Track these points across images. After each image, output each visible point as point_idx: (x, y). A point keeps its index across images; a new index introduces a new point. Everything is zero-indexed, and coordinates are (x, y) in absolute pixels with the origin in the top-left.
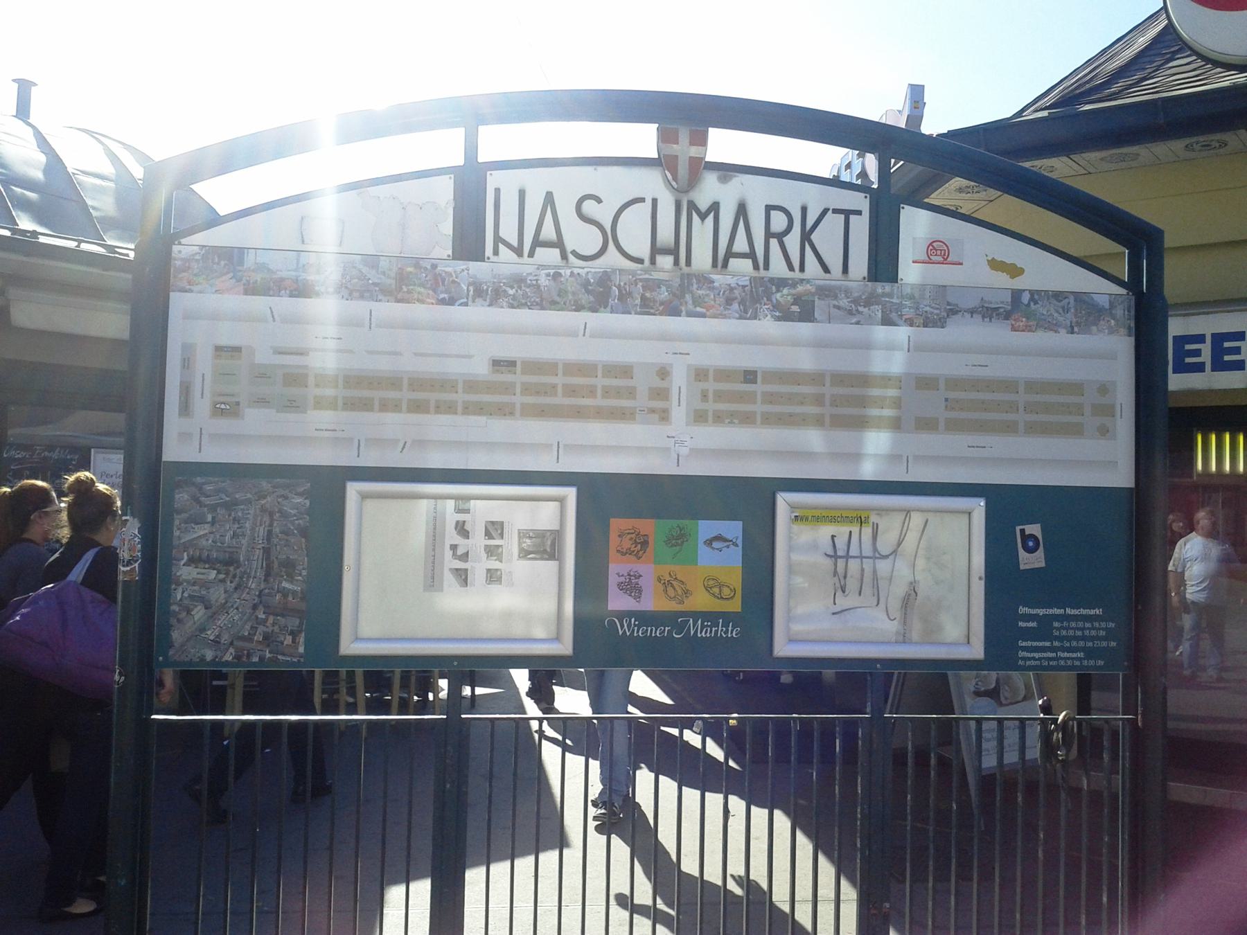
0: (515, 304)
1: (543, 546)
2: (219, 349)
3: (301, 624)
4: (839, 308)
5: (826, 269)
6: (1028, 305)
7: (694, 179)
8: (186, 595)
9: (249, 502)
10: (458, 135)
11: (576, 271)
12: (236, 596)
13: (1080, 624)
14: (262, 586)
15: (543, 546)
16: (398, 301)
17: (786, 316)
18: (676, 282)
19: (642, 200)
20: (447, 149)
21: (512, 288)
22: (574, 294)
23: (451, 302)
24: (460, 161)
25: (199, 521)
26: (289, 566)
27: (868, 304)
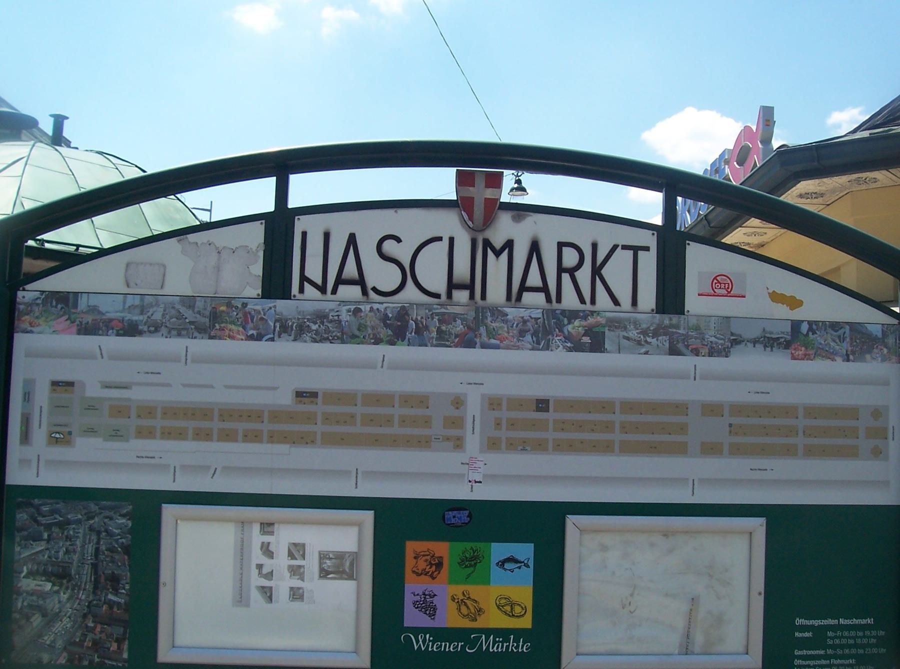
0: (318, 338)
1: (336, 567)
2: (55, 384)
3: (125, 633)
4: (628, 339)
5: (616, 302)
6: (807, 334)
7: (489, 220)
8: (25, 604)
9: (79, 522)
10: (270, 183)
11: (376, 306)
12: (68, 605)
13: (853, 633)
14: (91, 598)
15: (336, 567)
16: (211, 338)
17: (578, 347)
18: (472, 314)
19: (440, 239)
20: (256, 196)
21: (315, 323)
22: (373, 328)
23: (259, 338)
24: (271, 208)
25: (37, 538)
26: (115, 580)
27: (655, 334)
